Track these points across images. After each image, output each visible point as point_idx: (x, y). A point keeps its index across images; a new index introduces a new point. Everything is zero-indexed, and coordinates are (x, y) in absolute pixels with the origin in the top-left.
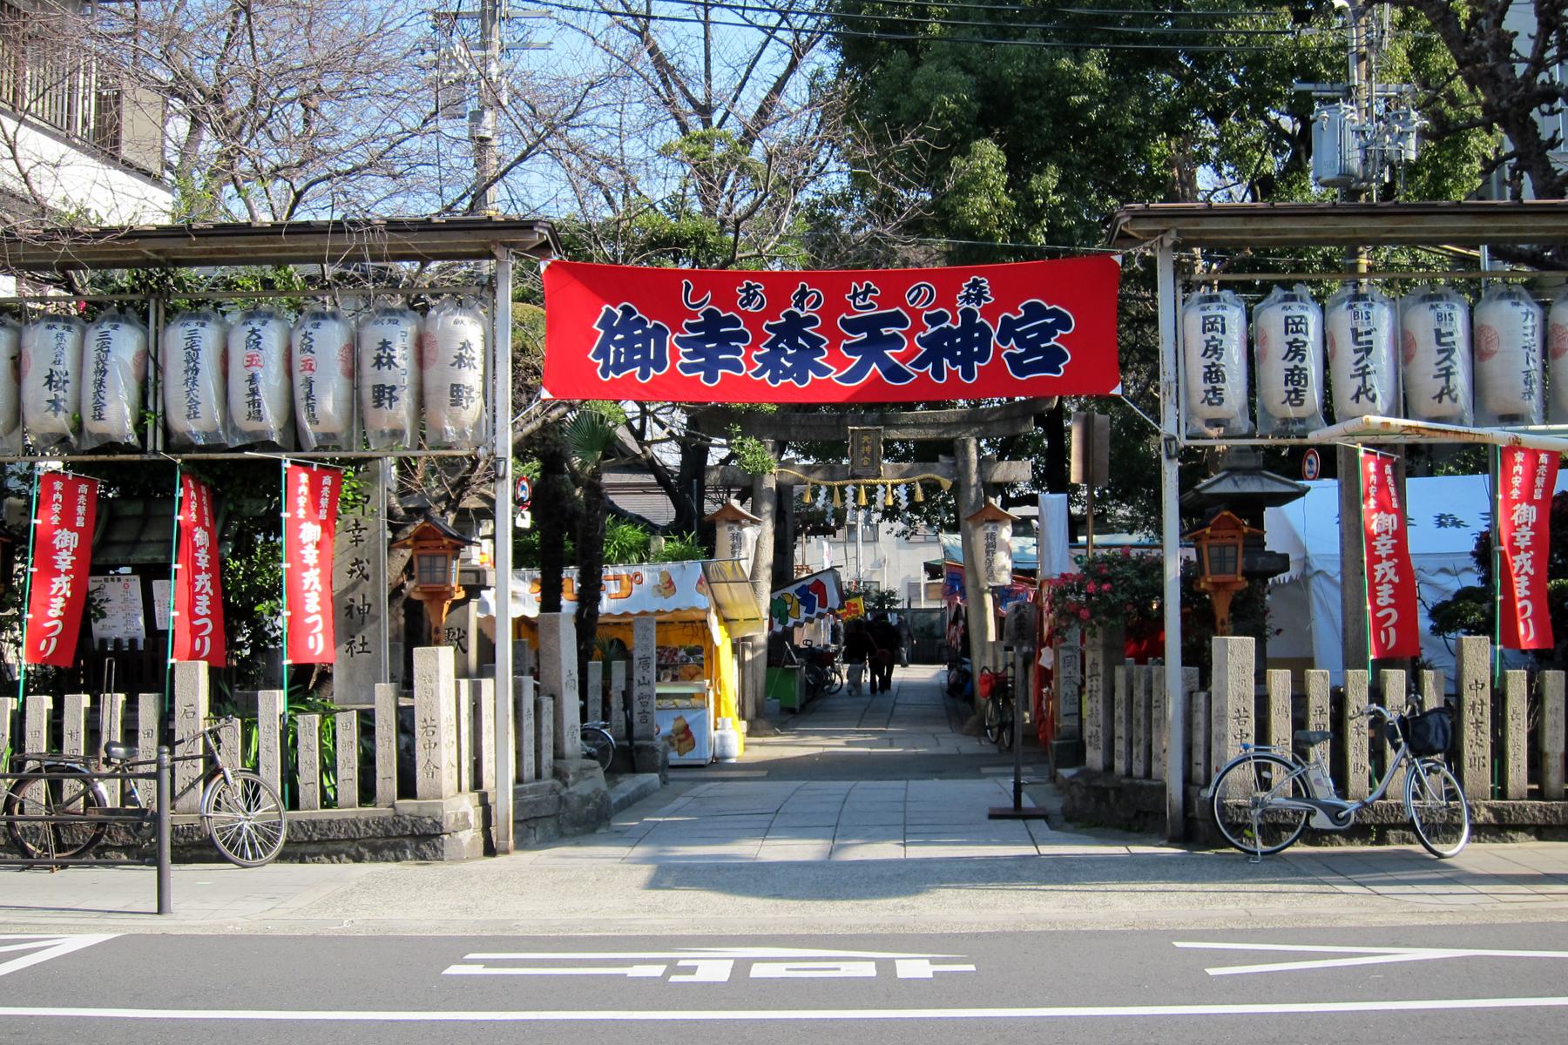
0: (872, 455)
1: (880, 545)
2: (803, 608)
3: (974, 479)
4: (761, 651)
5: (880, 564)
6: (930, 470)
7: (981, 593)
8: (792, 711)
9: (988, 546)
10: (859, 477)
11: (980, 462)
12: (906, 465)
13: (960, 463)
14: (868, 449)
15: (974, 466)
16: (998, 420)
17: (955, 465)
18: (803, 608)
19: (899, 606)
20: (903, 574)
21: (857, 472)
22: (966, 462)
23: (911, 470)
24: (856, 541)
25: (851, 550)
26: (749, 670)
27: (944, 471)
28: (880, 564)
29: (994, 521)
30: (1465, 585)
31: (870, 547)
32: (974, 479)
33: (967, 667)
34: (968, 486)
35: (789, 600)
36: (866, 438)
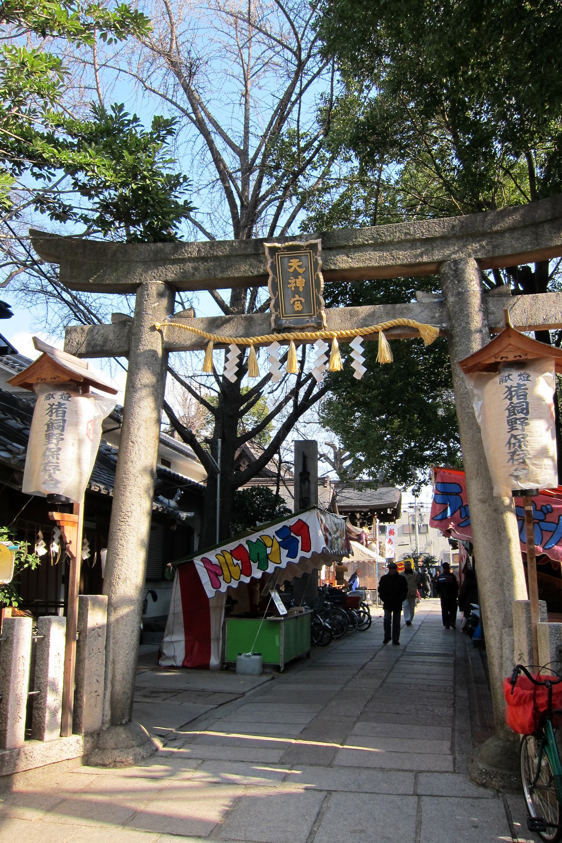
0: (306, 292)
1: (429, 534)
2: (284, 552)
3: (477, 320)
4: (124, 611)
5: (429, 544)
6: (402, 314)
7: (497, 511)
8: (277, 668)
9: (512, 410)
10: (288, 330)
11: (485, 293)
12: (364, 310)
13: (451, 299)
14: (300, 282)
15: (475, 301)
16: (512, 229)
17: (442, 304)
18: (284, 552)
19: (437, 564)
20: (441, 549)
21: (285, 322)
22: (462, 297)
23: (372, 315)
24: (415, 533)
25: (413, 537)
26: (96, 645)
27: (426, 314)
28: (429, 544)
29: (520, 365)
30: (377, 586)
31: (424, 536)
32: (477, 320)
33: (476, 612)
34: (468, 333)
35: (268, 543)
36: (295, 263)
